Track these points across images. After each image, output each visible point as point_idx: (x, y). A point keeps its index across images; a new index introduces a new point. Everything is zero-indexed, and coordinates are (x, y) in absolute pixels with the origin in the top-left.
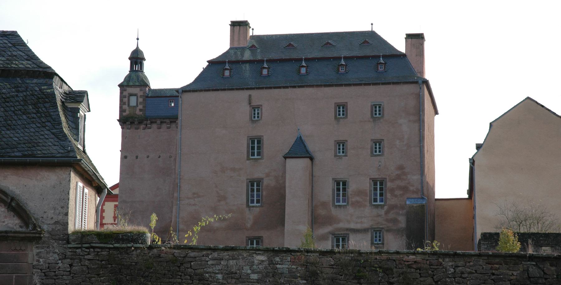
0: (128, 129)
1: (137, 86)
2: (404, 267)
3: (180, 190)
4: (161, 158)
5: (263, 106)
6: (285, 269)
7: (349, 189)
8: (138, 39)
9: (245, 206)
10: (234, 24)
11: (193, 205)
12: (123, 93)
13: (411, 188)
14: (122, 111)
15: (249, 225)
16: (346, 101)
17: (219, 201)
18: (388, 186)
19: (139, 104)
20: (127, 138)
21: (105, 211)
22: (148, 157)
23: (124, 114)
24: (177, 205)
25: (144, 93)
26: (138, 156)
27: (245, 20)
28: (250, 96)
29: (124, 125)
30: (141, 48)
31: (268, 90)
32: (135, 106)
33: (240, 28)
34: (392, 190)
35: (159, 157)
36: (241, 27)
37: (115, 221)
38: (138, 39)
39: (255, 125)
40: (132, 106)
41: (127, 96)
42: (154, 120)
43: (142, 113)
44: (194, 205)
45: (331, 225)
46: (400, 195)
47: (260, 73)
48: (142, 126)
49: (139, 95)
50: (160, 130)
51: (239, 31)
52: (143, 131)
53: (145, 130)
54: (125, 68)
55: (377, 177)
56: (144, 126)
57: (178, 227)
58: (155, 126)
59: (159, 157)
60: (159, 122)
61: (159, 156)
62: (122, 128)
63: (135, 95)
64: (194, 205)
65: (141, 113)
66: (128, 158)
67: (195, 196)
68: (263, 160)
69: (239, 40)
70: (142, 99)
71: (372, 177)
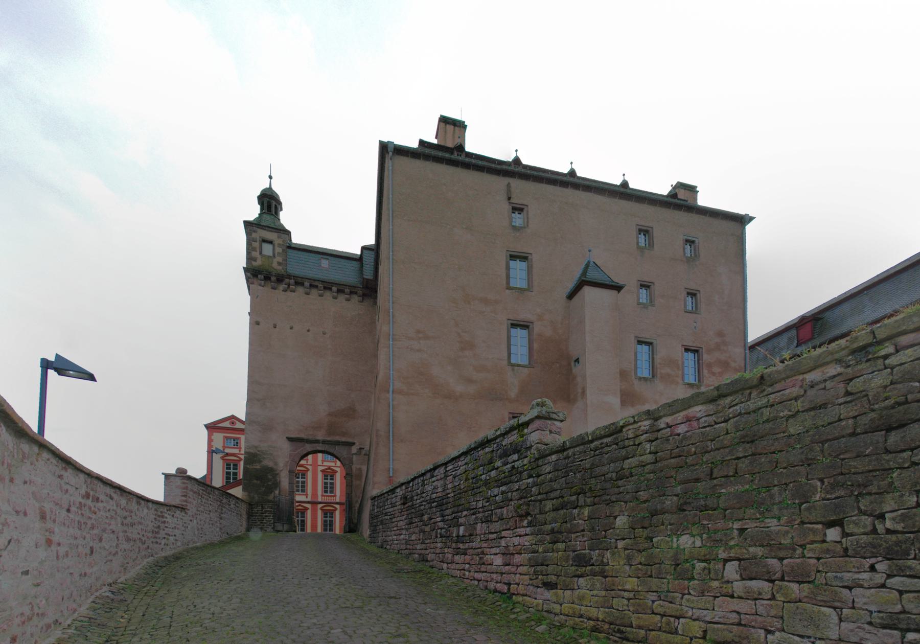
0: (260, 285)
5: (529, 207)
7: (656, 355)
8: (270, 177)
9: (505, 362)
12: (251, 235)
13: (733, 364)
14: (250, 258)
15: (513, 393)
16: (650, 225)
18: (704, 359)
23: (254, 264)
28: (509, 185)
30: (274, 188)
33: (454, 130)
34: (709, 366)
38: (270, 177)
39: (518, 234)
40: (264, 256)
42: (299, 280)
44: (419, 351)
45: (633, 406)
46: (719, 373)
48: (282, 286)
53: (286, 293)
54: (253, 211)
55: (690, 344)
58: (300, 290)
59: (308, 331)
60: (307, 284)
64: (419, 351)
65: (281, 268)
67: (421, 335)
68: (533, 293)
71: (685, 344)
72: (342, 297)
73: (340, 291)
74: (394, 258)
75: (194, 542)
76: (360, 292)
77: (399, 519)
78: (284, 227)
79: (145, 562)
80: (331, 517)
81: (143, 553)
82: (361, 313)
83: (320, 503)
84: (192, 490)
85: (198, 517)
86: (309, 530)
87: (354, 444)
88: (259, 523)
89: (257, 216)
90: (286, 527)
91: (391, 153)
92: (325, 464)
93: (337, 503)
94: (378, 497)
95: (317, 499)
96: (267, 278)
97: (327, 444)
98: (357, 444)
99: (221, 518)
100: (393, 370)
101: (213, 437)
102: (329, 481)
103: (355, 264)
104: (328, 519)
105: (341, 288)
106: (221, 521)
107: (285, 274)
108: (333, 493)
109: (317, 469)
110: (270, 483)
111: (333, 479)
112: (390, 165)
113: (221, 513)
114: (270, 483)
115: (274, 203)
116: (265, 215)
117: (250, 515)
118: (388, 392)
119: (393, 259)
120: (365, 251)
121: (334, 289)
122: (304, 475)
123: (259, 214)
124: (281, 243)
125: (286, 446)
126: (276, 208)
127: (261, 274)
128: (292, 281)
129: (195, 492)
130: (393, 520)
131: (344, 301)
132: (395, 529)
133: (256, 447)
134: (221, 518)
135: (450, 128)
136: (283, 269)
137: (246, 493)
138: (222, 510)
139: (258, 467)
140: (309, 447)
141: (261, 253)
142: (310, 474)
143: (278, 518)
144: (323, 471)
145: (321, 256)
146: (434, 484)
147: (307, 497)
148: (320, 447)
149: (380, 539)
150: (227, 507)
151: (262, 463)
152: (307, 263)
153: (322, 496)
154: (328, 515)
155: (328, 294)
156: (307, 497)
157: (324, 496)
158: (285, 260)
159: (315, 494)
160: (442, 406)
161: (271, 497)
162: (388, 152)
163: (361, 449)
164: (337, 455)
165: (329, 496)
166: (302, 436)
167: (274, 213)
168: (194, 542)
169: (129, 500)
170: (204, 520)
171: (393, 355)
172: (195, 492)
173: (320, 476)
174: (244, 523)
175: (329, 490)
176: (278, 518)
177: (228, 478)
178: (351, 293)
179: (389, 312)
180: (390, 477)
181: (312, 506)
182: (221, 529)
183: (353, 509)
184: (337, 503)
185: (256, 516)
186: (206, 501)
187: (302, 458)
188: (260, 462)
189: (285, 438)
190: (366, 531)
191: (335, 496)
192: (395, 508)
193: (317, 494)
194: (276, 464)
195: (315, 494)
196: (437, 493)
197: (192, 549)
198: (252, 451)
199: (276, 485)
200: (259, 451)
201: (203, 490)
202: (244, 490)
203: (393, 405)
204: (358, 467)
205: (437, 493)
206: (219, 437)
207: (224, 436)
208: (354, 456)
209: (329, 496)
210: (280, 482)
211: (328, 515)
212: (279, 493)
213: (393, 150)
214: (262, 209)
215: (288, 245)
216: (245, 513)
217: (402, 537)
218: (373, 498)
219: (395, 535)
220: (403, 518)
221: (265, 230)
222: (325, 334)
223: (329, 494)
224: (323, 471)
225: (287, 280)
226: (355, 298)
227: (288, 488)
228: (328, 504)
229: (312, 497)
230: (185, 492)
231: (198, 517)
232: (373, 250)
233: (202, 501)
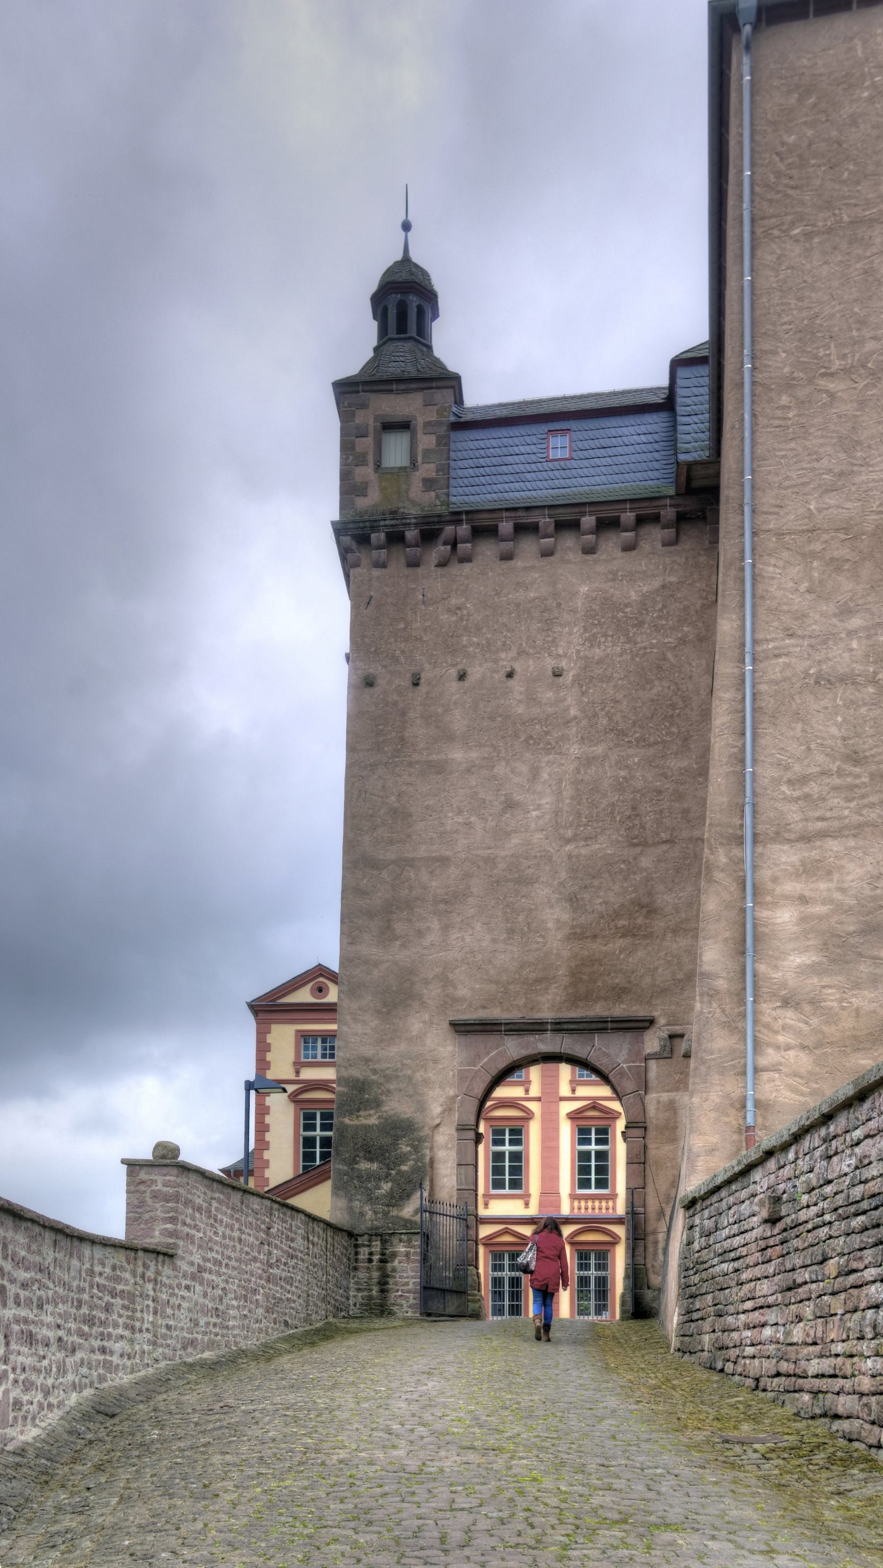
1: (414, 386)
2: (478, 655)
4: (516, 677)
6: (636, 822)
8: (406, 226)
12: (353, 415)
19: (420, 459)
20: (373, 602)
22: (462, 677)
23: (362, 503)
25: (440, 413)
26: (422, 675)
29: (360, 552)
30: (416, 257)
32: (405, 468)
35: (510, 675)
37: (298, 1073)
38: (406, 226)
41: (371, 430)
42: (484, 520)
43: (433, 494)
47: (755, 398)
49: (420, 420)
50: (512, 563)
52: (440, 570)
56: (442, 548)
58: (488, 550)
59: (510, 675)
60: (506, 527)
61: (509, 669)
62: (257, 1023)
63: (404, 426)
66: (381, 682)
70: (433, 438)
72: (611, 543)
73: (607, 524)
74: (759, 376)
76: (668, 513)
77: (758, 1271)
78: (443, 367)
79: (74, 1398)
80: (599, 1267)
81: (70, 1377)
82: (673, 579)
83: (568, 1221)
87: (651, 1022)
89: (371, 354)
91: (747, 29)
92: (582, 1091)
93: (619, 1221)
94: (704, 1198)
95: (558, 1206)
96: (396, 538)
98: (662, 1021)
102: (593, 1147)
103: (655, 423)
104: (592, 1273)
105: (608, 513)
107: (440, 510)
108: (606, 1187)
109: (557, 1113)
110: (404, 1168)
111: (604, 1141)
112: (746, 68)
114: (404, 1168)
115: (413, 301)
116: (391, 347)
118: (740, 841)
119: (753, 383)
120: (681, 372)
121: (588, 521)
122: (517, 1135)
123: (376, 349)
124: (433, 417)
126: (421, 312)
127: (374, 529)
128: (464, 530)
130: (744, 1276)
131: (618, 553)
132: (749, 1305)
136: (437, 497)
137: (342, 1203)
139: (373, 1121)
141: (378, 466)
142: (534, 1131)
144: (573, 1116)
145: (544, 428)
146: (857, 1150)
147: (527, 1205)
148: (546, 1044)
149: (706, 1338)
151: (384, 1109)
152: (510, 459)
153: (573, 1197)
154: (593, 1262)
155: (569, 542)
156: (527, 1205)
157: (580, 1198)
158: (445, 469)
159: (550, 1192)
162: (737, 29)
163: (672, 1037)
164: (598, 1064)
165: (593, 1198)
166: (496, 1013)
167: (414, 335)
169: (33, 1238)
170: (222, 1285)
171: (754, 710)
173: (566, 1131)
175: (593, 1177)
177: (309, 1157)
178: (641, 521)
179: (742, 569)
180: (748, 1129)
183: (650, 1238)
184: (619, 1221)
186: (228, 1232)
187: (499, 1079)
188: (377, 1104)
189: (446, 1025)
190: (672, 1315)
191: (613, 1196)
192: (748, 1236)
193: (558, 1194)
194: (422, 1107)
195: (550, 1192)
196: (865, 1182)
200: (375, 1072)
201: (219, 1201)
202: (336, 1189)
204: (665, 1096)
205: (865, 1182)
208: (653, 1064)
209: (593, 1198)
210: (432, 1161)
211: (593, 1262)
213: (752, 17)
214: (383, 331)
215: (453, 419)
217: (768, 1332)
218: (691, 1204)
219: (747, 1327)
220: (771, 1268)
221: (390, 391)
222: (560, 675)
223: (593, 1191)
224: (573, 1116)
225: (449, 530)
226: (655, 535)
228: (591, 1224)
229: (541, 1205)
230: (172, 1210)
232: (703, 361)
233: (216, 1233)
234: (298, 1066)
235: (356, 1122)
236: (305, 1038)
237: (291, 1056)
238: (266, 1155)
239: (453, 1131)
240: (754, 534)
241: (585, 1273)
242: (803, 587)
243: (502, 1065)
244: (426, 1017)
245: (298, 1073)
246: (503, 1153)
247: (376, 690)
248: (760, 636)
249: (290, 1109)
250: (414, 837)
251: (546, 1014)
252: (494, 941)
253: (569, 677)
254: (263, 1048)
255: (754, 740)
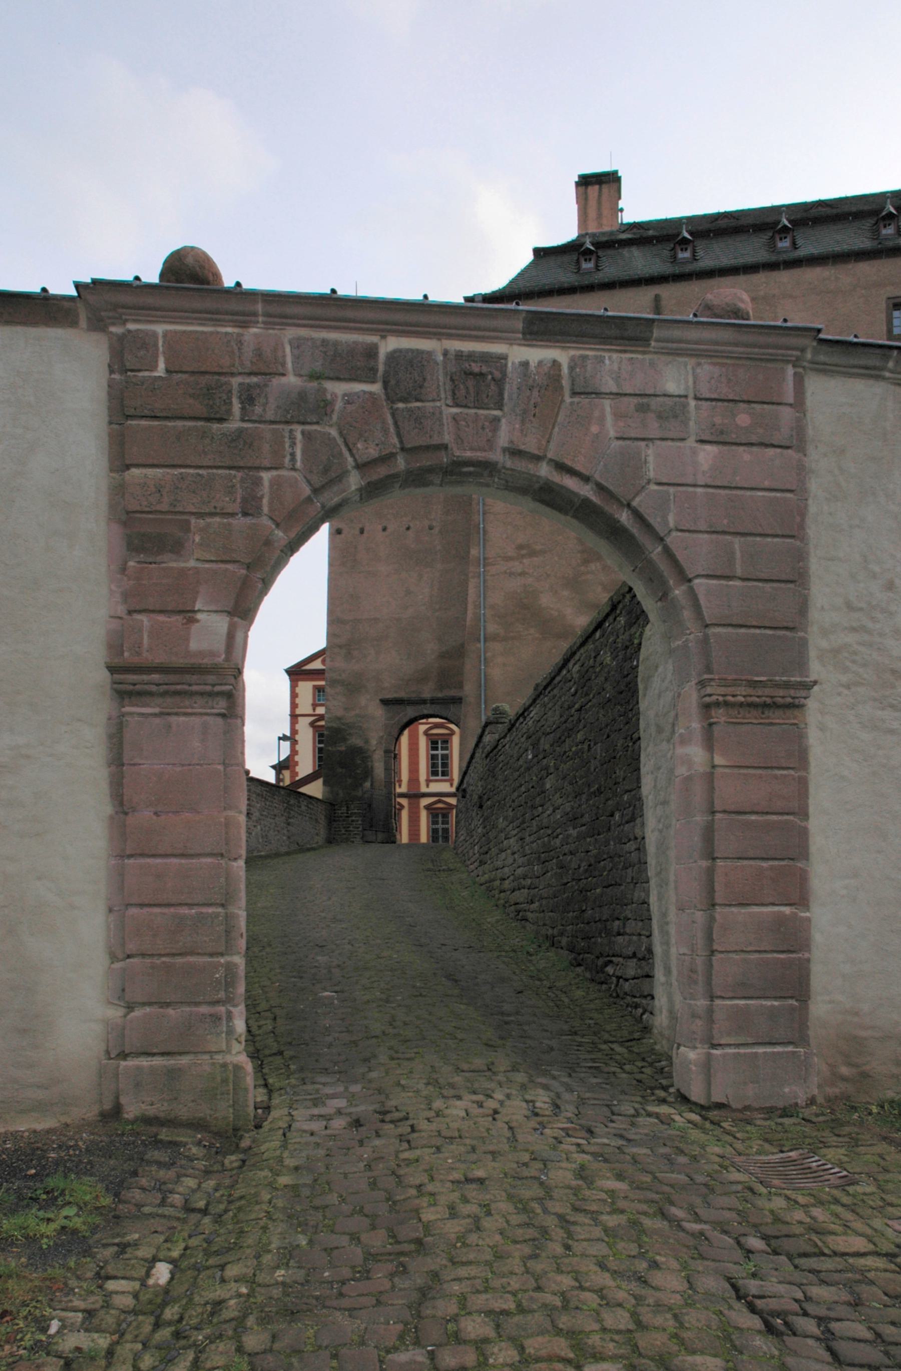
3: (484, 540)
4: (411, 530)
10: (585, 182)
11: (520, 574)
17: (586, 562)
21: (300, 696)
22: (384, 529)
24: (479, 577)
27: (614, 169)
28: (657, 299)
31: (704, 281)
33: (600, 190)
35: (408, 529)
36: (604, 186)
37: (314, 710)
44: (523, 574)
51: (600, 196)
57: (485, 629)
59: (408, 529)
64: (523, 574)
66: (345, 532)
67: (524, 552)
69: (600, 216)
75: (259, 851)
84: (255, 792)
85: (262, 822)
86: (405, 838)
88: (343, 832)
90: (380, 836)
97: (438, 703)
99: (289, 824)
100: (485, 608)
101: (298, 690)
106: (290, 828)
113: (289, 818)
117: (331, 820)
125: (378, 712)
129: (258, 795)
133: (339, 719)
134: (289, 824)
135: (593, 190)
138: (289, 813)
139: (343, 748)
140: (411, 712)
143: (370, 825)
147: (452, 785)
150: (296, 809)
160: (554, 651)
161: (360, 793)
166: (402, 695)
168: (259, 851)
172: (258, 795)
174: (323, 832)
176: (370, 825)
181: (410, 804)
182: (289, 837)
185: (339, 821)
188: (345, 740)
189: (378, 701)
194: (367, 742)
197: (256, 857)
198: (334, 725)
199: (368, 773)
200: (343, 724)
202: (325, 783)
203: (485, 659)
206: (306, 688)
207: (315, 687)
210: (372, 767)
212: (372, 785)
216: (323, 817)
227: (383, 776)
231: (262, 822)
234: (315, 706)
235: (334, 749)
236: (319, 690)
237: (310, 701)
238: (297, 758)
239: (382, 753)
240: (484, 514)
241: (436, 826)
242: (504, 536)
243: (405, 720)
244: (368, 697)
245: (314, 710)
246: (437, 755)
247: (343, 536)
248: (487, 556)
249: (310, 730)
250: (520, 336)
251: (427, 695)
252: (401, 659)
253: (436, 531)
254: (294, 695)
255: (484, 599)
